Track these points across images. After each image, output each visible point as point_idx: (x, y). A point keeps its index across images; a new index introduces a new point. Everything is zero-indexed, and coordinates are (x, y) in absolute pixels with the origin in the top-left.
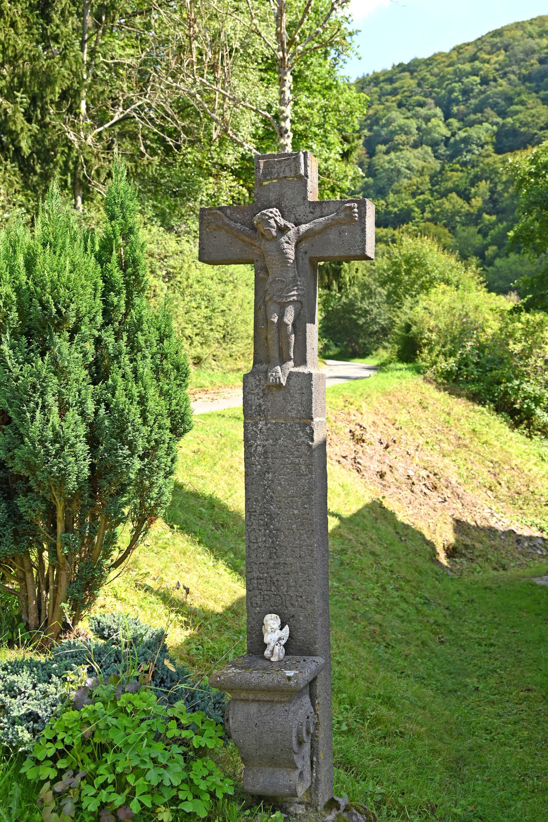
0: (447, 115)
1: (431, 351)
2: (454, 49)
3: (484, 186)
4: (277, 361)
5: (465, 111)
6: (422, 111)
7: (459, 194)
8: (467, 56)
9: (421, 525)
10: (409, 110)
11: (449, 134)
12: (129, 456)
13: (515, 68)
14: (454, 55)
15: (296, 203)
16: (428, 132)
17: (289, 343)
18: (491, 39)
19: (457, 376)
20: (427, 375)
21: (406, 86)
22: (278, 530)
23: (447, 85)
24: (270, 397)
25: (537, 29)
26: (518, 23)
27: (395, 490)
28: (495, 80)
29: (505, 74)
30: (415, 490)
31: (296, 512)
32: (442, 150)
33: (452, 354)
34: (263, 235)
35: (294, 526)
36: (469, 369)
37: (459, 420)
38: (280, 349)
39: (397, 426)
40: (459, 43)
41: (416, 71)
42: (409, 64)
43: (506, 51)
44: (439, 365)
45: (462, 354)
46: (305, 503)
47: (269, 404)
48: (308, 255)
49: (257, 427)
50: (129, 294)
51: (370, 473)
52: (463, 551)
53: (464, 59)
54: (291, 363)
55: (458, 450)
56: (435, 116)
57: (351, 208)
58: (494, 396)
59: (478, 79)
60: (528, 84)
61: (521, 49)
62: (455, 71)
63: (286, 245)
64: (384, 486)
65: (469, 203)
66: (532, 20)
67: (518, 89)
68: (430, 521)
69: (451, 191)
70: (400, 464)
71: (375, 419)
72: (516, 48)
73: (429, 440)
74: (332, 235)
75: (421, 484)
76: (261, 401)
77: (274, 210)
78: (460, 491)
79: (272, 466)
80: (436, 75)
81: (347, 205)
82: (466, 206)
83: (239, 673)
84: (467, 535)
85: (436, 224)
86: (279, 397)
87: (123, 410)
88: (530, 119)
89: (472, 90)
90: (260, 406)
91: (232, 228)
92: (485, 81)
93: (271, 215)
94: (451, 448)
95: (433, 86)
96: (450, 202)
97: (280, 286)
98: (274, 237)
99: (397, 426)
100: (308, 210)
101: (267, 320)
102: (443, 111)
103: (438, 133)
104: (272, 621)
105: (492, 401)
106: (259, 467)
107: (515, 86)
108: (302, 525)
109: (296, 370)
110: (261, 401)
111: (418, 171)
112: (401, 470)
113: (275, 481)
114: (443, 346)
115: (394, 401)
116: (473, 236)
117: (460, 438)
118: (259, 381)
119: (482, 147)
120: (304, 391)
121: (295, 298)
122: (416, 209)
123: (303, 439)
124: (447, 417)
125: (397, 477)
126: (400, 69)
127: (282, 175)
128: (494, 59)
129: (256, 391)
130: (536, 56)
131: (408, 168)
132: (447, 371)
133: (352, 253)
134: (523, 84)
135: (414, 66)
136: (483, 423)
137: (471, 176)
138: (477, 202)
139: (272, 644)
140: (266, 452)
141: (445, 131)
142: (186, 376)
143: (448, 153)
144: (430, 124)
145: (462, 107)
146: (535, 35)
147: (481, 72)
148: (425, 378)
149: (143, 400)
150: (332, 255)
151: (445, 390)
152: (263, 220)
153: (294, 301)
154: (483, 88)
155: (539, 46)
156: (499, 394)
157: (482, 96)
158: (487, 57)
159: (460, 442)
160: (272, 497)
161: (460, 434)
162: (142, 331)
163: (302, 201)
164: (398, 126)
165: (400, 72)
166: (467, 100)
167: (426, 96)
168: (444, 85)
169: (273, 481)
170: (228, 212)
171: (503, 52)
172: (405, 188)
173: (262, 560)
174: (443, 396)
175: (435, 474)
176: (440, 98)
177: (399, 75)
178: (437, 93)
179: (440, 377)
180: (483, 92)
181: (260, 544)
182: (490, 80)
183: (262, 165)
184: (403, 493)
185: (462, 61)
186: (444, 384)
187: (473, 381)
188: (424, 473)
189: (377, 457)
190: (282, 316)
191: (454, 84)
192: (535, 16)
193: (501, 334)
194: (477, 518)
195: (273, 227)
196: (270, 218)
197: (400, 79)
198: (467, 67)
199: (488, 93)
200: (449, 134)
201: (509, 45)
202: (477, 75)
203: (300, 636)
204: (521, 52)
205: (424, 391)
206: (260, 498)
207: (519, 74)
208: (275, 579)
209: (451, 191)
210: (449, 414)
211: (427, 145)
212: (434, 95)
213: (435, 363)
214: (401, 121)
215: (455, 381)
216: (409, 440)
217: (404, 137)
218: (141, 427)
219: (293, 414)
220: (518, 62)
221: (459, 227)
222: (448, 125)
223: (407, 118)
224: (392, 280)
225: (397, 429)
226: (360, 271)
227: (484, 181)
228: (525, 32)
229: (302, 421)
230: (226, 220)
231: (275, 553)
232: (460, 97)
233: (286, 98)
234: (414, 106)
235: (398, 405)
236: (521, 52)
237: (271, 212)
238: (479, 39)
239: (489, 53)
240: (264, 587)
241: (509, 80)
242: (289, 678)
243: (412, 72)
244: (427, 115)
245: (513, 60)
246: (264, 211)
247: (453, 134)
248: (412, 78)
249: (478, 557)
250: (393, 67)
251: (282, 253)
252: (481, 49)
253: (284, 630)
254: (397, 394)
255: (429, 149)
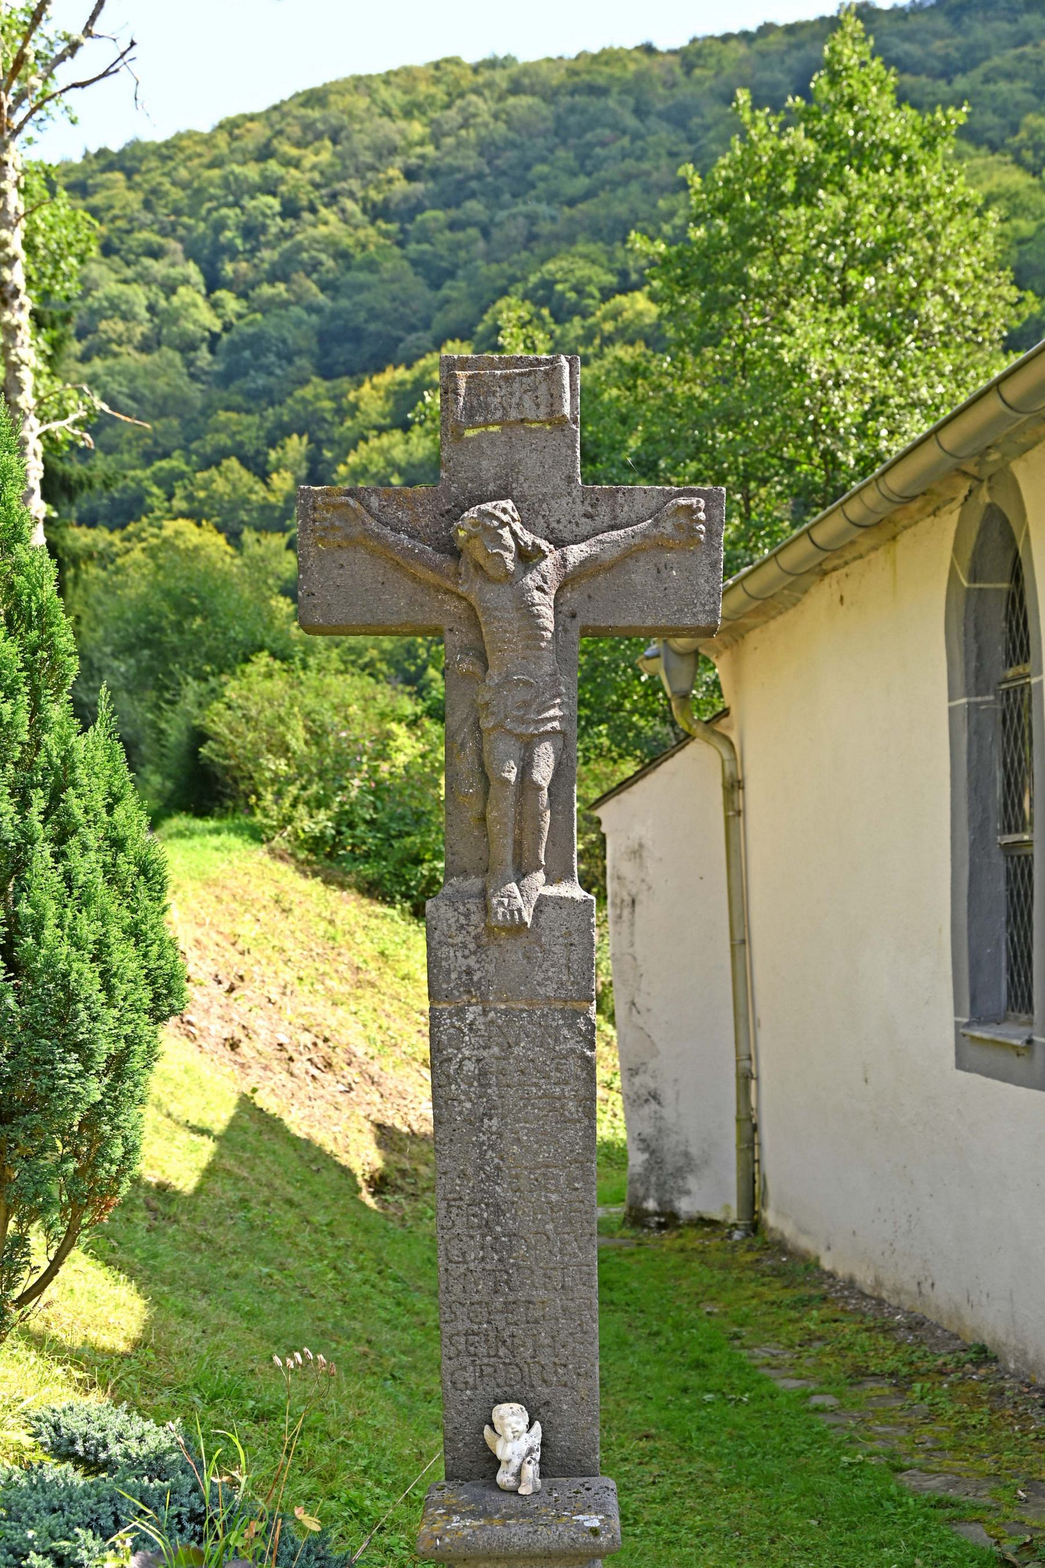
0: (213, 283)
1: (279, 795)
2: (221, 126)
3: (296, 446)
4: (510, 871)
5: (251, 275)
6: (158, 268)
7: (244, 461)
8: (251, 146)
9: (323, 1138)
10: (128, 264)
11: (217, 327)
12: (80, 1075)
13: (354, 184)
14: (222, 140)
15: (548, 490)
16: (173, 317)
17: (539, 830)
18: (303, 111)
19: (334, 847)
20: (273, 844)
21: (118, 204)
22: (512, 1235)
23: (210, 211)
24: (494, 952)
25: (402, 98)
26: (359, 79)
27: (261, 1073)
28: (313, 210)
29: (333, 199)
30: (296, 1072)
31: (554, 1197)
32: (203, 357)
33: (320, 803)
34: (478, 567)
35: (550, 1227)
36: (358, 832)
37: (352, 934)
38: (518, 844)
39: (240, 947)
40: (232, 113)
41: (138, 171)
42: (122, 153)
43: (335, 141)
44: (298, 824)
45: (342, 804)
46: (576, 1179)
47: (491, 968)
48: (579, 622)
49: (462, 1020)
50: (35, 694)
51: (211, 1040)
52: (399, 1182)
53: (244, 151)
54: (540, 876)
55: (359, 992)
56: (186, 281)
57: (691, 510)
58: (409, 888)
59: (275, 203)
60: (382, 225)
61: (367, 141)
62: (225, 178)
63: (537, 594)
64: (242, 1065)
65: (267, 484)
66: (388, 73)
67: (361, 234)
68: (336, 1129)
69: (224, 453)
70: (260, 1022)
71: (198, 933)
72: (356, 137)
73: (302, 974)
74: (640, 575)
75: (305, 1058)
76: (472, 961)
77: (509, 504)
78: (374, 1069)
79: (499, 1103)
80: (184, 186)
81: (682, 501)
82: (259, 487)
83: (482, 1528)
84: (401, 1151)
85: (199, 525)
86: (514, 952)
87: (65, 975)
88: (387, 305)
89: (264, 228)
90: (469, 972)
91: (388, 546)
92: (290, 210)
93: (506, 518)
94: (346, 988)
95: (177, 212)
96: (227, 479)
97: (521, 695)
98: (508, 574)
99: (240, 947)
100: (580, 509)
101: (485, 778)
102: (203, 271)
103: (195, 322)
104: (511, 1417)
105: (406, 896)
106: (468, 1105)
107: (356, 227)
108: (569, 1222)
109: (552, 891)
110: (472, 961)
111: (154, 405)
112: (264, 1034)
113: (507, 1134)
114: (304, 788)
115: (226, 896)
116: (276, 554)
117: (358, 968)
118: (467, 916)
119: (290, 362)
120: (575, 939)
121: (556, 724)
122: (155, 490)
123: (571, 1044)
124: (331, 929)
125: (260, 1047)
126: (103, 162)
127: (514, 415)
128: (310, 159)
129: (459, 939)
130: (399, 161)
131: (132, 397)
132: (314, 838)
133: (688, 621)
134: (373, 222)
135: (134, 158)
136: (397, 939)
137: (268, 425)
138: (283, 482)
139: (516, 1462)
140: (483, 1073)
141: (208, 319)
142: (161, 890)
143: (216, 368)
144: (175, 300)
145: (244, 265)
146: (396, 111)
147: (283, 188)
148: (271, 851)
149: (100, 952)
150: (639, 623)
151: (315, 874)
152: (486, 528)
153: (554, 732)
154: (288, 224)
155: (405, 137)
156: (419, 883)
157: (287, 245)
158: (294, 152)
159: (361, 976)
160: (498, 1168)
161: (358, 961)
162: (74, 785)
163: (563, 485)
164: (107, 298)
165: (104, 170)
166: (253, 251)
167: (163, 232)
168: (203, 212)
169: (500, 1135)
170: (374, 502)
171: (328, 143)
172: (129, 443)
173: (477, 1298)
174: (314, 886)
175: (326, 1040)
176: (195, 241)
177: (101, 178)
178: (188, 228)
179: (300, 847)
180: (287, 236)
181: (472, 1266)
182: (302, 209)
183: (462, 384)
184: (276, 1078)
185: (239, 157)
186: (308, 862)
187: (366, 856)
188: (307, 1039)
189: (216, 1010)
190: (526, 768)
191: (224, 211)
192: (395, 66)
193: (424, 765)
194: (411, 1118)
195: (507, 548)
196: (503, 524)
197: (103, 186)
198: (251, 172)
199: (299, 237)
200: (217, 326)
201: (342, 128)
202: (274, 194)
203: (562, 1440)
204: (367, 148)
205: (277, 877)
206: (470, 1171)
207: (365, 199)
208: (506, 1334)
209: (224, 453)
210: (331, 922)
211: (171, 346)
212: (181, 231)
213: (289, 820)
214: (113, 288)
215: (329, 856)
216: (266, 975)
217: (121, 326)
218: (104, 1011)
219: (550, 990)
220: (360, 171)
221: (248, 536)
222: (215, 305)
223: (125, 281)
224: (147, 643)
225: (242, 953)
226: (84, 622)
227: (295, 437)
228: (374, 101)
229: (568, 1006)
230: (373, 524)
231: (506, 1282)
232: (239, 242)
233: (11, 209)
234: (138, 255)
235: (235, 905)
236: (367, 148)
237: (504, 511)
238: (275, 108)
239: (299, 144)
240: (482, 1350)
241: (343, 211)
242: (595, 1532)
243: (129, 173)
244: (168, 277)
245: (352, 165)
246: (488, 506)
247: (227, 327)
248: (130, 188)
249: (425, 1190)
250: (86, 156)
251: (528, 613)
252: (280, 133)
253: (533, 1430)
254: (228, 883)
255: (176, 357)
